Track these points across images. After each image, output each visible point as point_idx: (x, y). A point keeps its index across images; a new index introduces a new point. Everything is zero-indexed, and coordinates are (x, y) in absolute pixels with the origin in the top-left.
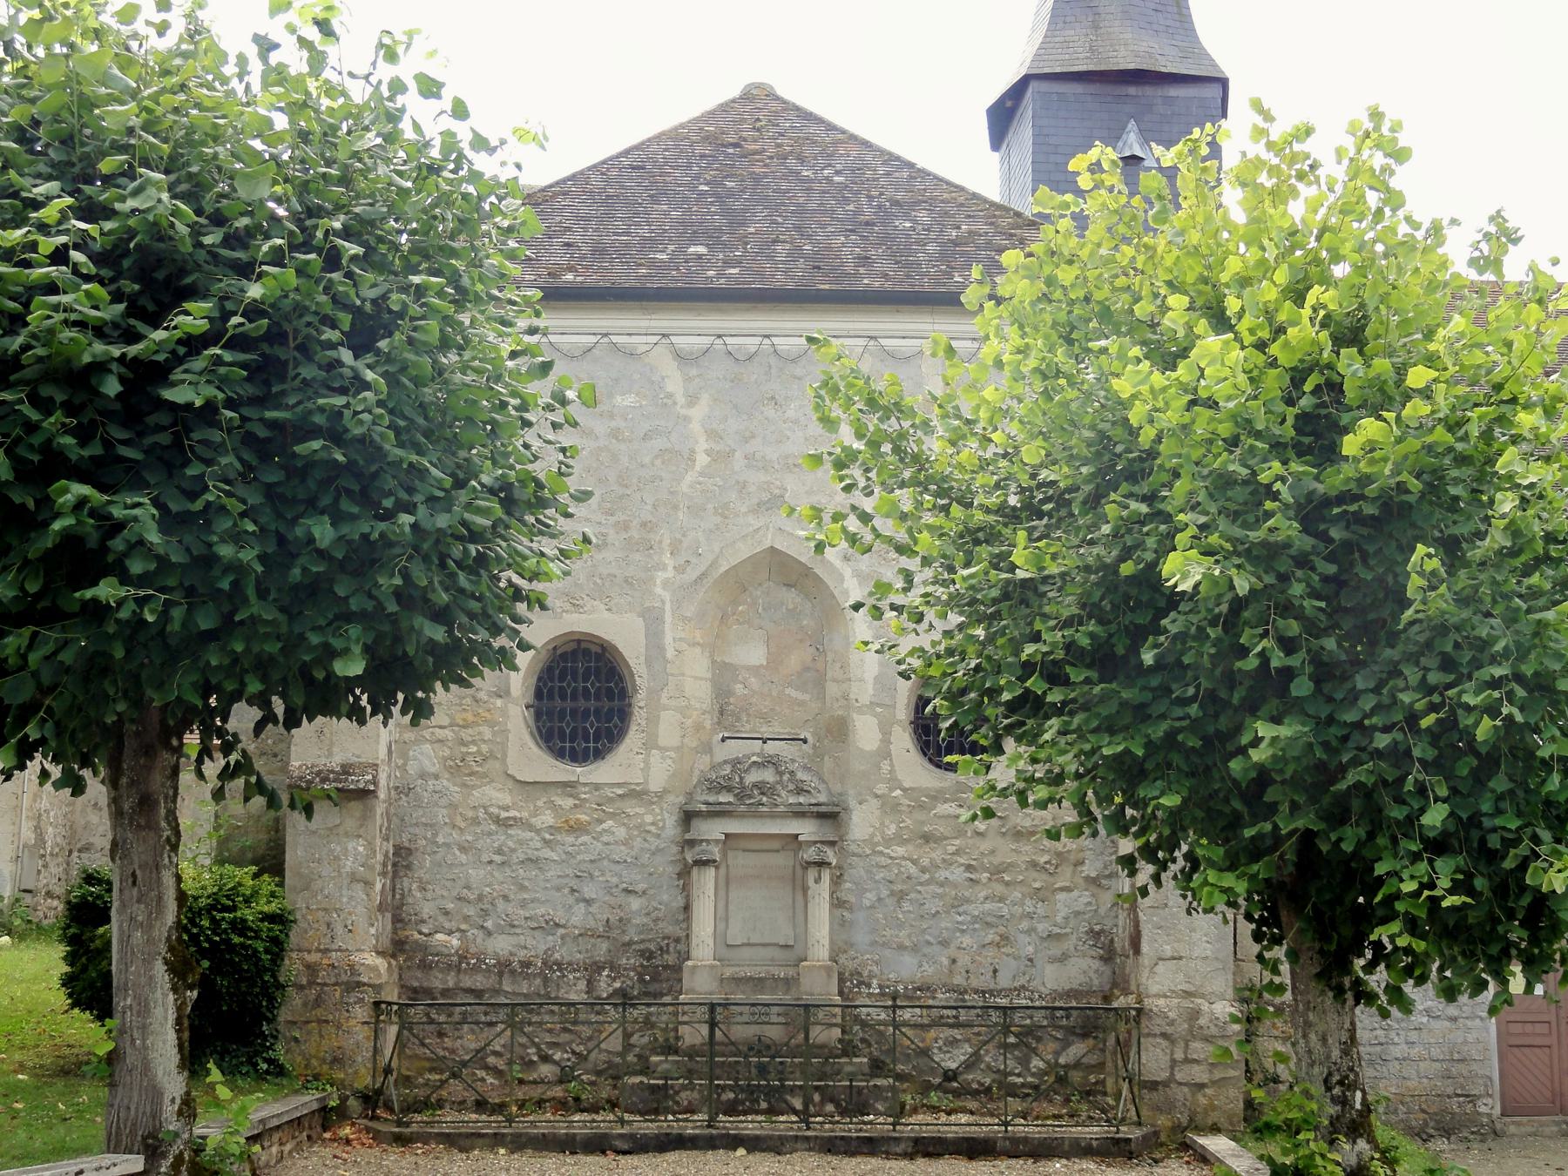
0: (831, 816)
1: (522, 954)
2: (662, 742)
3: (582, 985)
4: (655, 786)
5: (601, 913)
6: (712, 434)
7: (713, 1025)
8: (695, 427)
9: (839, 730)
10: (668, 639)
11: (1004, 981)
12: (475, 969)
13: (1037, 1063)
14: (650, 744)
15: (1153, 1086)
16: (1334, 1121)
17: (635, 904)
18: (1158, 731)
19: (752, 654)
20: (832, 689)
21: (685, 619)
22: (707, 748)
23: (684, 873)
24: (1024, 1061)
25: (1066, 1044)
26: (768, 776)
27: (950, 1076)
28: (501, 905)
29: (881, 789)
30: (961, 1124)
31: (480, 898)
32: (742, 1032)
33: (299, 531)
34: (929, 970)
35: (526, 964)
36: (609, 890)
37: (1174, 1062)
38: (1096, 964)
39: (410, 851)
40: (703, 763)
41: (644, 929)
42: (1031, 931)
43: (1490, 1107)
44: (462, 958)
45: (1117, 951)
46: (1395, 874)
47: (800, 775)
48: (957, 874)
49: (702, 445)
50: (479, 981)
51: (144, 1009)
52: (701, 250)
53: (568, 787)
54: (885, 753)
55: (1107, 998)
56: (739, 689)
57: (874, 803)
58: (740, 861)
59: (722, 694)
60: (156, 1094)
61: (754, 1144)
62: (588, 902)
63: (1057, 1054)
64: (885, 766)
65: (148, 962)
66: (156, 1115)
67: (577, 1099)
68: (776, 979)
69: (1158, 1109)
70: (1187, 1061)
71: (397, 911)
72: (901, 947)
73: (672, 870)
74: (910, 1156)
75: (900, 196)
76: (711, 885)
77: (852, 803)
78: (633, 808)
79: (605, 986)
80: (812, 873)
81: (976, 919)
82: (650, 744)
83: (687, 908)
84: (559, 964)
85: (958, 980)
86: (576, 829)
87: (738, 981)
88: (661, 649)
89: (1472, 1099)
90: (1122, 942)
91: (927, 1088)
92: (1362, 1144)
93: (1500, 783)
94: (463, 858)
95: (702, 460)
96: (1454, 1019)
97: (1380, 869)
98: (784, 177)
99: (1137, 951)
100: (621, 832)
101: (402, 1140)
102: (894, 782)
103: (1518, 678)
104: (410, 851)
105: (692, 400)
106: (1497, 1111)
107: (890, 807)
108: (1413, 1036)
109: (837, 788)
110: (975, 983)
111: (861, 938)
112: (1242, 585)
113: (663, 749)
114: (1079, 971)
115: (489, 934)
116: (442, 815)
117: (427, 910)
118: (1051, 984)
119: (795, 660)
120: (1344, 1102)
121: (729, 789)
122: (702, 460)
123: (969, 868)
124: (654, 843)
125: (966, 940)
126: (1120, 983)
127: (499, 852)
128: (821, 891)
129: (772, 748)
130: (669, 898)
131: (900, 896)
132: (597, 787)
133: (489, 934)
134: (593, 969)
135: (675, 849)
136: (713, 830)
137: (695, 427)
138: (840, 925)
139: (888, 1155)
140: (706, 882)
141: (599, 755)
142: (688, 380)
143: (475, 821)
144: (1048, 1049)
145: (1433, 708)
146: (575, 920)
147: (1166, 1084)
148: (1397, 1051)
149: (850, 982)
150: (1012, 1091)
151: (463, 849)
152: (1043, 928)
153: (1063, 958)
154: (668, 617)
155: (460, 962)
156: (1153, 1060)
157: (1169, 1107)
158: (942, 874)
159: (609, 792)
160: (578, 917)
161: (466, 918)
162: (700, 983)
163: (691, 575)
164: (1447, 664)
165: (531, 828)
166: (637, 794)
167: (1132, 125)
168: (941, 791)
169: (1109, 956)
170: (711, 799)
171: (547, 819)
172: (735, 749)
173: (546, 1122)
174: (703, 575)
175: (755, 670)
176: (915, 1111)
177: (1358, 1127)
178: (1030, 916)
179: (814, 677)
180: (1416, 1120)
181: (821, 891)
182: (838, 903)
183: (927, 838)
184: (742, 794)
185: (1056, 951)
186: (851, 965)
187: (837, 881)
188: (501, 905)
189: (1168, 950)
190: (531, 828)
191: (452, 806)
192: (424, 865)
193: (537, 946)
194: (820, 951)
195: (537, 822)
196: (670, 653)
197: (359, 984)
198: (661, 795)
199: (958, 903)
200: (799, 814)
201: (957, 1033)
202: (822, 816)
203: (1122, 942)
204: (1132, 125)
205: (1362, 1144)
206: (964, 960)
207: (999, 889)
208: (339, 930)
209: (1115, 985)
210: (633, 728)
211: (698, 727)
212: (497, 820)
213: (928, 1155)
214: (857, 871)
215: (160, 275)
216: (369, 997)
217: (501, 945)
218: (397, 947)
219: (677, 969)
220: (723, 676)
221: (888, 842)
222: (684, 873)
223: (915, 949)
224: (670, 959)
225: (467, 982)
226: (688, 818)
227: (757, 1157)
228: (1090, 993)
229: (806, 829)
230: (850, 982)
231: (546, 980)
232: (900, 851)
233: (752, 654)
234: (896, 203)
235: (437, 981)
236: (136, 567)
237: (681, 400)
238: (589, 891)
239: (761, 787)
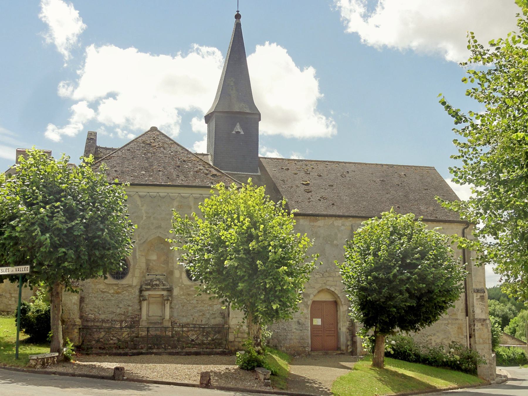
0: (170, 290)
1: (107, 318)
2: (136, 275)
3: (119, 324)
4: (134, 284)
5: (122, 311)
6: (147, 213)
7: (148, 331)
8: (143, 211)
9: (171, 273)
10: (137, 255)
11: (203, 323)
12: (97, 321)
13: (210, 339)
14: (133, 276)
15: (231, 342)
16: (255, 344)
17: (130, 308)
18: (226, 283)
19: (154, 257)
20: (170, 265)
21: (141, 251)
22: (144, 277)
23: (140, 302)
24: (207, 338)
25: (215, 335)
26: (158, 283)
27: (193, 340)
28: (102, 308)
29: (180, 285)
30: (194, 350)
31: (98, 307)
32: (152, 333)
33: (93, 252)
34: (189, 320)
35: (108, 320)
36: (124, 305)
37: (235, 337)
38: (221, 319)
39: (84, 298)
40: (144, 279)
41: (131, 313)
42: (209, 313)
43: (308, 349)
44: (94, 319)
45: (225, 316)
46: (258, 305)
47: (164, 282)
48: (195, 302)
49: (145, 215)
50: (98, 324)
51: (57, 329)
52: (144, 172)
53: (116, 285)
54: (181, 277)
55: (223, 326)
56: (151, 264)
57: (178, 288)
58: (151, 300)
59: (148, 265)
60: (59, 342)
61: (156, 354)
62: (120, 308)
63: (213, 337)
64: (181, 281)
65: (58, 321)
66: (59, 346)
67: (119, 347)
68: (158, 322)
69: (232, 346)
70: (238, 337)
71: (81, 309)
72: (183, 316)
73: (137, 301)
74: (185, 355)
75: (185, 159)
76: (146, 305)
77: (174, 287)
78: (130, 289)
79: (124, 325)
80: (166, 302)
81: (198, 310)
82: (133, 276)
83: (140, 309)
84: (114, 320)
85: (194, 323)
86: (118, 293)
87: (151, 323)
88: (136, 257)
89: (304, 347)
90: (226, 315)
91: (188, 343)
92: (259, 347)
93: (272, 293)
94: (95, 299)
95: (144, 218)
96: (301, 330)
97: (256, 305)
98: (161, 153)
99: (229, 316)
100: (127, 294)
101: (88, 354)
102: (182, 283)
103: (273, 278)
104: (84, 298)
105: (142, 206)
106: (310, 350)
107: (181, 289)
108: (293, 334)
109: (171, 284)
110: (198, 323)
111: (175, 314)
112: (236, 264)
113: (136, 277)
114: (219, 320)
115: (100, 314)
116: (90, 291)
117: (87, 310)
118: (212, 323)
119: (162, 259)
120: (257, 341)
121: (150, 285)
122: (144, 218)
123: (197, 300)
124: (134, 296)
125: (196, 315)
126: (226, 323)
127: (102, 298)
128: (168, 306)
129: (158, 277)
130: (137, 307)
131: (183, 306)
132: (122, 285)
133: (100, 314)
134: (121, 322)
135: (138, 297)
136: (146, 293)
137: (143, 211)
138: (171, 312)
139: (181, 355)
140: (145, 304)
141: (122, 278)
142: (142, 201)
143: (97, 292)
144: (212, 335)
145: (263, 282)
146: (118, 312)
147: (234, 342)
148: (288, 337)
149: (173, 323)
150: (204, 344)
151: (95, 297)
152: (211, 312)
153: (215, 318)
154: (137, 250)
155: (94, 320)
156: (231, 337)
157: (234, 346)
158: (191, 302)
159: (125, 286)
160: (118, 311)
161: (95, 311)
162: (144, 323)
163: (142, 241)
164: (265, 275)
165: (109, 293)
166: (130, 286)
167: (238, 124)
168: (192, 285)
169: (224, 317)
170: (146, 287)
171: (112, 291)
172: (150, 277)
173: (114, 351)
174: (144, 242)
175: (154, 261)
176: (186, 347)
177: (258, 344)
178: (209, 310)
179: (166, 262)
180: (293, 352)
181: (168, 306)
182: (171, 308)
183: (189, 295)
184: (153, 286)
185: (213, 316)
186: (173, 320)
187: (171, 303)
188: (102, 308)
189: (235, 316)
190: (109, 293)
191: (93, 289)
192: (87, 301)
193: (110, 317)
194: (167, 317)
195: (110, 292)
196: (138, 257)
197: (76, 325)
198: (135, 286)
199: (195, 307)
200: (163, 290)
201: (194, 333)
202: (168, 291)
203: (226, 315)
204: (238, 124)
205: (259, 347)
206: (195, 319)
207: (203, 305)
208: (72, 314)
209: (225, 323)
210: (130, 272)
211: (143, 272)
212: (102, 292)
213: (188, 355)
214: (175, 302)
215: (70, 211)
216: (78, 327)
217: (103, 317)
218: (81, 317)
219: (139, 321)
220: (148, 262)
221: (181, 295)
222: (140, 302)
223: (186, 316)
224: (137, 319)
225: (96, 324)
226: (141, 291)
227: (156, 356)
228: (220, 325)
229: (165, 293)
230: (173, 323)
231: (112, 324)
232: (183, 297)
233: (154, 257)
234: (184, 161)
235: (90, 324)
236: (69, 260)
237: (140, 206)
238: (121, 306)
239: (156, 285)
